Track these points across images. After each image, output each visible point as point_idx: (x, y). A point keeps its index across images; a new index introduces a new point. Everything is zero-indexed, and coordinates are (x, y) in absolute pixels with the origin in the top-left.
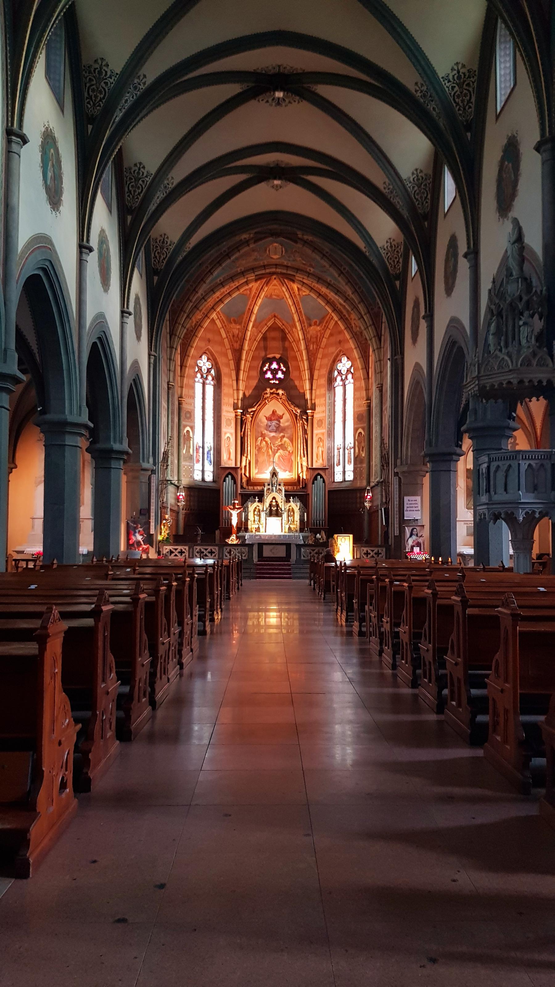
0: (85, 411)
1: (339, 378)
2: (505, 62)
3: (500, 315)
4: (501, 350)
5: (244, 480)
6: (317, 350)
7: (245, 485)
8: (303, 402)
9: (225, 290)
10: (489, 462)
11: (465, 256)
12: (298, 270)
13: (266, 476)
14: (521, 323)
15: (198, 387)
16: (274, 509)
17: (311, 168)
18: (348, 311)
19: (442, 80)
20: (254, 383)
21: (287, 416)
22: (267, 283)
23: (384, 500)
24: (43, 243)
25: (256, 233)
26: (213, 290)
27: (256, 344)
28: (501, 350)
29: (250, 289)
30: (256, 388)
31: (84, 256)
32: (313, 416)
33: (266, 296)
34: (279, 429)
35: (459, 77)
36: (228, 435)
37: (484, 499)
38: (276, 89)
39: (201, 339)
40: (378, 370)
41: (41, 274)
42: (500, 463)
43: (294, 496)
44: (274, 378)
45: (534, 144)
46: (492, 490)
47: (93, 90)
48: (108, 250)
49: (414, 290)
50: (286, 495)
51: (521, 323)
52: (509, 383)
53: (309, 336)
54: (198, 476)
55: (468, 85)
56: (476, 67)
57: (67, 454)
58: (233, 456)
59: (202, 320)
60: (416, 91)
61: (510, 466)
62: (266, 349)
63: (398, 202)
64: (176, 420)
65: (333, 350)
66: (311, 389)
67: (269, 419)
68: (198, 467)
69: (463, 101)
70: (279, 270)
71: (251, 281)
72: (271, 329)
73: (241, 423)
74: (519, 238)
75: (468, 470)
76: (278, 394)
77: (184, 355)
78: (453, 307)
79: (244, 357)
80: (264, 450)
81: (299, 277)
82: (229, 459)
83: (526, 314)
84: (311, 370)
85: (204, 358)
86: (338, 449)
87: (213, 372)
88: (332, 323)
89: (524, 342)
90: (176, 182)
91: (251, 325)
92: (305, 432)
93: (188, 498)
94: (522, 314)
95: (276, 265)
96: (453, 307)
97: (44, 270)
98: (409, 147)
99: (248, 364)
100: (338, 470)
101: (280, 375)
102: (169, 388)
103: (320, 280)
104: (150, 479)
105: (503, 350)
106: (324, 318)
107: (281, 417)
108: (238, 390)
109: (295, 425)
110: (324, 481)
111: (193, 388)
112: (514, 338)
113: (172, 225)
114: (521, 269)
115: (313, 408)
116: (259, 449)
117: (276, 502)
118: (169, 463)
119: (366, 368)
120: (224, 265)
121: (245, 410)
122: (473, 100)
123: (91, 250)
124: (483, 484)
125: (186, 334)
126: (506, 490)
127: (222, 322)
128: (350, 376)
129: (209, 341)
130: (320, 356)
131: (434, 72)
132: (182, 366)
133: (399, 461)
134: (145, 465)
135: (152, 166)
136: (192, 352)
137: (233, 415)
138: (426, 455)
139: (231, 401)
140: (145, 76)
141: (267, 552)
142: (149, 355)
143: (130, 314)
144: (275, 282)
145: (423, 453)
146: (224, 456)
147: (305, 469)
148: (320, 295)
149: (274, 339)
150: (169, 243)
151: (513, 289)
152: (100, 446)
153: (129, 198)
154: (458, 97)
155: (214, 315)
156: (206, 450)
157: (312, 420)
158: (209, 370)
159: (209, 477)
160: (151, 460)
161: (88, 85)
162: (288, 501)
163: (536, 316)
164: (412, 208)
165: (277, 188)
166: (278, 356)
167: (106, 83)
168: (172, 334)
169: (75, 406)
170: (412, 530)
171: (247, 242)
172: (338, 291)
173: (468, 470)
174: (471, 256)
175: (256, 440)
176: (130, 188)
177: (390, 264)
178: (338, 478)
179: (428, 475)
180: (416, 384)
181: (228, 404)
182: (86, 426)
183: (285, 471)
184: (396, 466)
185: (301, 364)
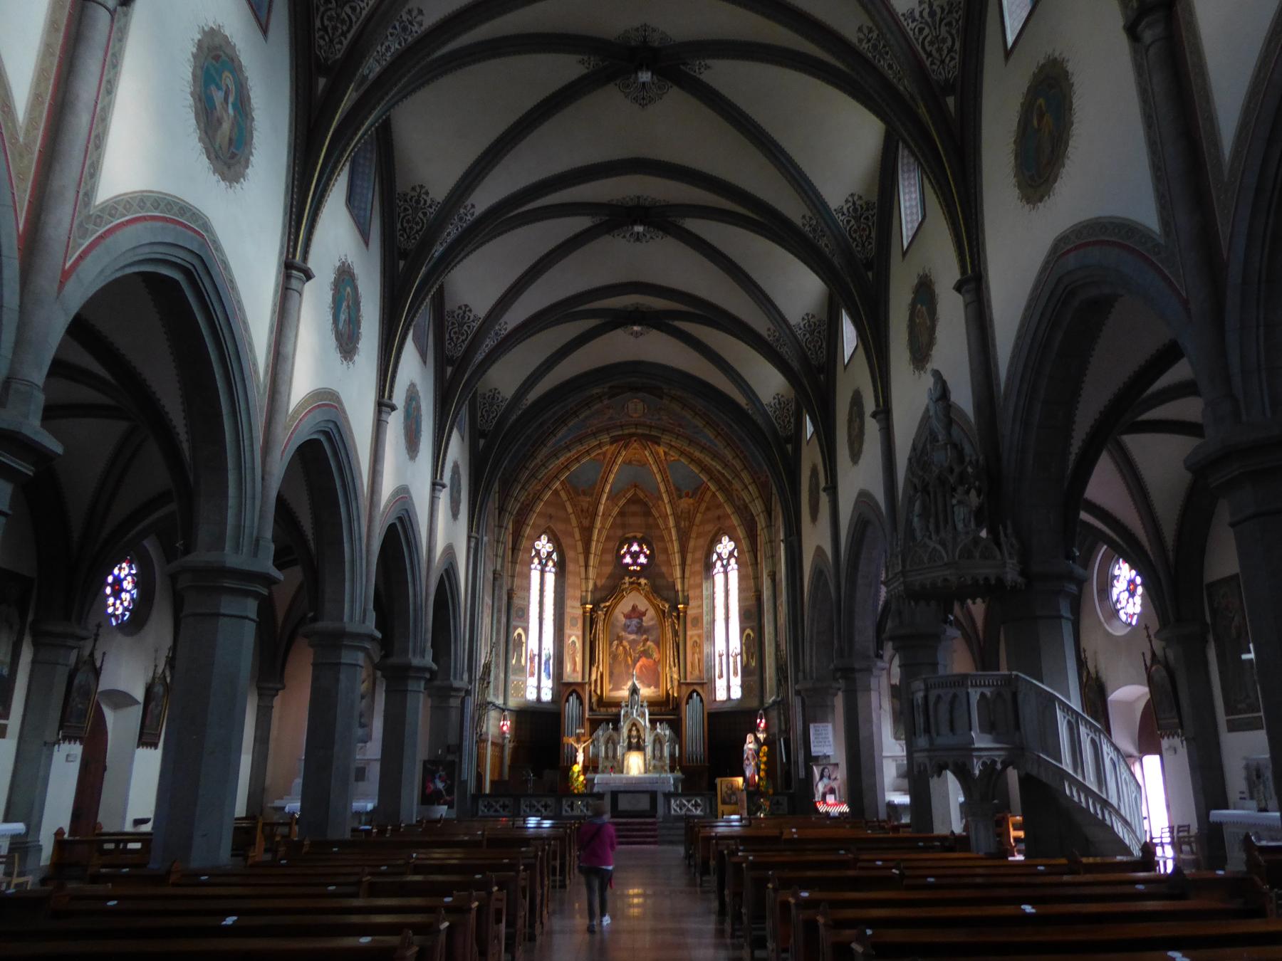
0: (372, 616)
1: (719, 564)
2: (910, 192)
3: (925, 490)
4: (930, 538)
5: (594, 699)
6: (690, 527)
7: (595, 706)
8: (672, 594)
9: (572, 454)
10: (927, 690)
11: (874, 415)
12: (664, 431)
13: (624, 693)
14: (954, 502)
15: (535, 576)
16: (634, 741)
17: (677, 313)
18: (728, 481)
19: (902, 19)
20: (608, 570)
21: (651, 612)
22: (626, 446)
23: (783, 727)
24: (327, 401)
25: (610, 387)
26: (555, 455)
27: (611, 520)
28: (930, 538)
29: (605, 454)
30: (611, 576)
31: (384, 416)
32: (685, 612)
33: (624, 462)
34: (640, 630)
35: (855, 210)
36: (573, 638)
37: (922, 742)
38: (635, 223)
39: (541, 514)
40: (769, 554)
41: (322, 439)
42: (941, 691)
43: (661, 722)
44: (635, 563)
45: (954, 282)
46: (933, 731)
47: (408, 222)
48: (418, 408)
49: (811, 456)
50: (651, 721)
51: (954, 502)
52: (945, 580)
53: (679, 510)
54: (531, 695)
55: (867, 218)
56: (875, 199)
57: (342, 677)
58: (579, 668)
59: (542, 492)
60: (860, 41)
61: (955, 696)
62: (623, 526)
63: (786, 351)
64: (504, 620)
65: (710, 528)
66: (683, 577)
67: (628, 616)
68: (532, 682)
69: (861, 237)
70: (639, 431)
71: (606, 444)
72: (630, 501)
73: (590, 622)
74: (942, 393)
75: (893, 687)
76: (639, 584)
77: (517, 535)
78: (860, 477)
79: (595, 537)
80: (621, 657)
81: (666, 438)
82: (572, 671)
83: (960, 489)
84: (683, 552)
85: (544, 539)
86: (721, 656)
87: (554, 556)
88: (709, 494)
89: (960, 526)
90: (510, 327)
91: (605, 496)
92: (676, 633)
93: (517, 727)
94: (954, 490)
95: (636, 425)
96: (860, 477)
97: (326, 434)
98: (799, 290)
99: (600, 547)
100: (720, 684)
101: (642, 560)
102: (495, 579)
103: (691, 442)
104: (463, 702)
105: (934, 537)
106: (698, 488)
107: (644, 614)
108: (587, 578)
109: (662, 625)
110: (701, 700)
111: (528, 577)
112: (946, 522)
113: (505, 378)
114: (949, 434)
115: (686, 603)
116: (614, 657)
117: (638, 731)
118: (492, 679)
119: (754, 550)
120: (570, 425)
121: (596, 604)
122: (873, 235)
123: (393, 408)
124: (920, 720)
125: (520, 509)
126: (952, 729)
127: (568, 493)
128: (733, 561)
129: (551, 517)
130: (693, 535)
131: (824, 204)
132: (515, 549)
133: (801, 675)
134: (457, 684)
135: (481, 308)
136: (528, 531)
137: (580, 612)
138: (837, 670)
139: (578, 594)
140: (473, 206)
141: (624, 804)
142: (469, 537)
143: (444, 486)
144: (635, 445)
145: (832, 666)
146: (568, 667)
147: (676, 683)
148: (692, 460)
149: (634, 514)
150: (429, 202)
151: (942, 458)
152: (394, 660)
153: (322, 42)
154: (855, 232)
155: (557, 485)
156: (543, 659)
157: (685, 617)
158: (549, 555)
159: (547, 696)
160: (466, 676)
161: (322, 9)
162: (653, 727)
163: (973, 493)
164: (804, 359)
165: (637, 335)
166: (639, 535)
167: (425, 214)
168: (502, 510)
169: (357, 608)
170: (823, 771)
171: (599, 398)
172: (715, 456)
173: (893, 687)
174: (881, 416)
175: (611, 644)
176: (326, 22)
177: (929, 55)
178: (721, 695)
179: (840, 694)
180: (818, 573)
181: (574, 598)
182: (372, 638)
183: (649, 686)
184: (797, 682)
185: (669, 546)
